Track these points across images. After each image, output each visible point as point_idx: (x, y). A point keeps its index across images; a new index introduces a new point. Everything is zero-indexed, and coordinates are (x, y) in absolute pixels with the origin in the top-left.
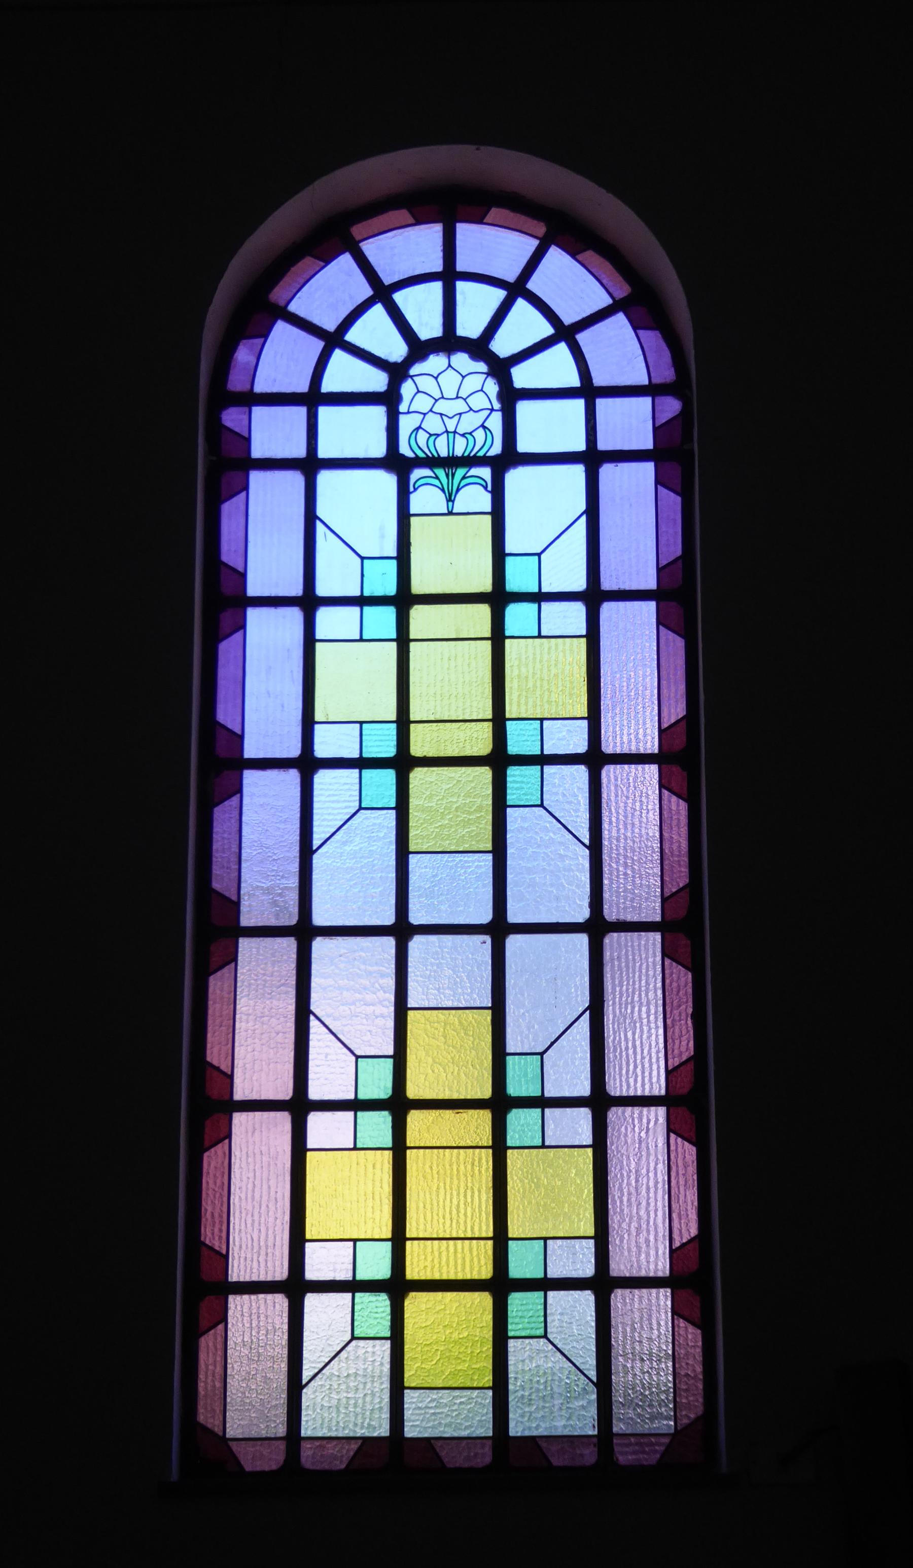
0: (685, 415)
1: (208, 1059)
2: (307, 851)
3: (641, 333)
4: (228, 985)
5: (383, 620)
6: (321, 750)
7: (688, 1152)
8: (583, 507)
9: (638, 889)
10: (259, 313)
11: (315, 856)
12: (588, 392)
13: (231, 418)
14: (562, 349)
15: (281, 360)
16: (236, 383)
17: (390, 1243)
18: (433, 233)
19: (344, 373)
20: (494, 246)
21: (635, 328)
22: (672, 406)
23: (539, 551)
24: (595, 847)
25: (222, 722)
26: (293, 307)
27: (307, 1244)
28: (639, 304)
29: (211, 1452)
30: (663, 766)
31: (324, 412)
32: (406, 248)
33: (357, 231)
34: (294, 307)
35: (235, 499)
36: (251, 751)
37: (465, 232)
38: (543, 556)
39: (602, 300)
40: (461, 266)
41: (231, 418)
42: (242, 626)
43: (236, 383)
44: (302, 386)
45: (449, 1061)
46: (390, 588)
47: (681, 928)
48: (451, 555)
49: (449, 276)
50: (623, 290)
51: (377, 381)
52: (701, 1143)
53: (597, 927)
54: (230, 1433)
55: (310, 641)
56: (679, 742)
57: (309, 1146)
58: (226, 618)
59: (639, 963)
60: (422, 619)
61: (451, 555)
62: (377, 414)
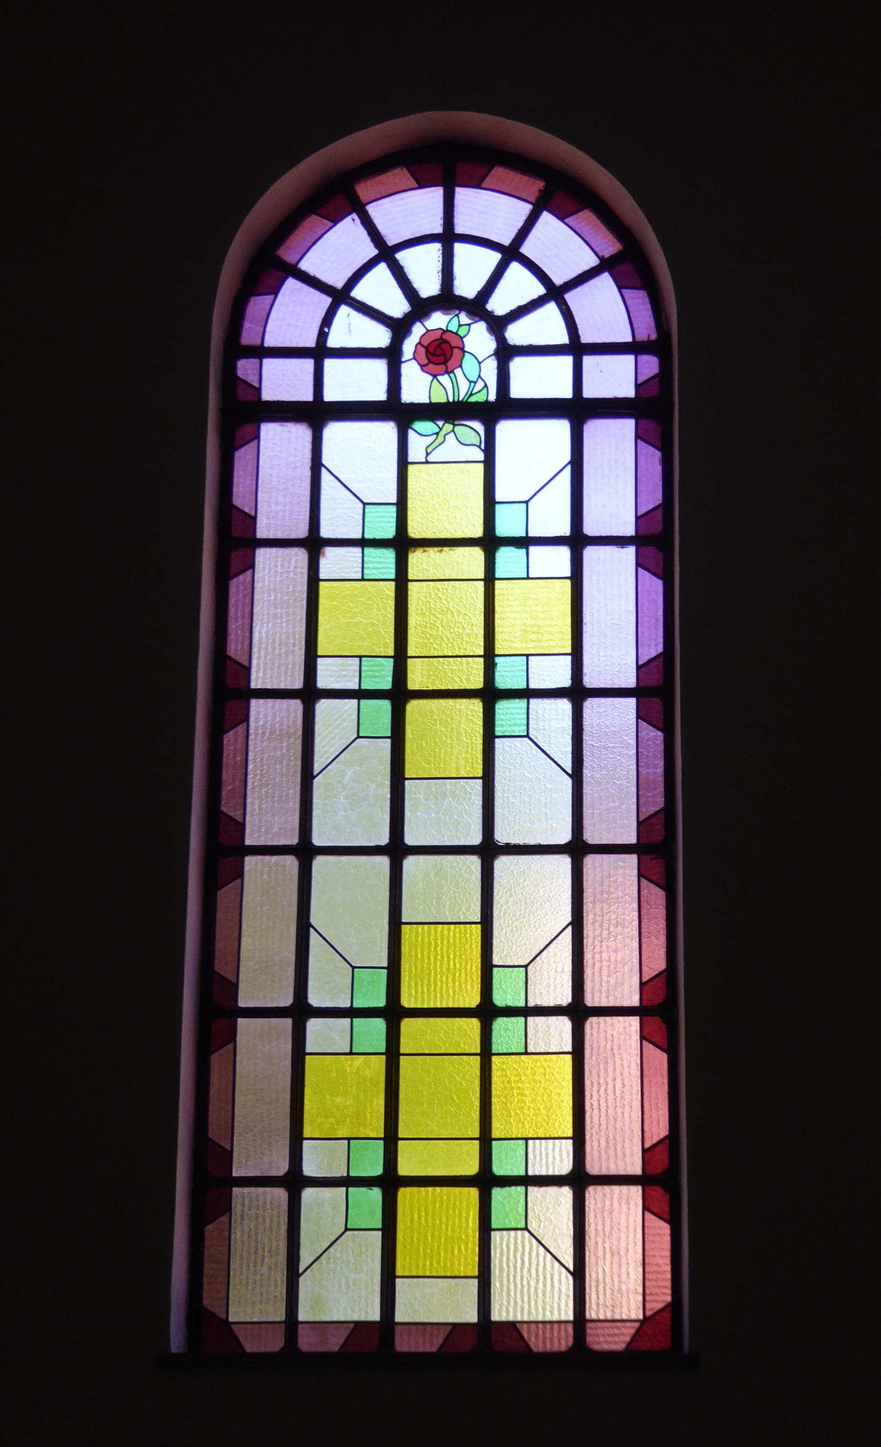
0: (664, 375)
1: (216, 969)
2: (307, 776)
3: (627, 293)
4: (251, 456)
5: (383, 561)
6: (324, 681)
7: (659, 1059)
8: (568, 458)
9: (616, 818)
10: (271, 269)
11: (301, 1279)
12: (577, 348)
13: (245, 368)
14: (552, 308)
15: (290, 315)
16: (248, 337)
17: (384, 1057)
18: (434, 196)
19: (350, 328)
20: (489, 210)
21: (620, 288)
22: (651, 365)
23: (527, 499)
24: (579, 1274)
25: (233, 656)
26: (304, 265)
27: (307, 1057)
28: (626, 266)
29: (210, 1328)
30: (646, 1188)
31: (330, 364)
32: (410, 210)
33: (363, 190)
34: (305, 265)
35: (223, 1050)
36: (263, 531)
37: (463, 195)
38: (530, 503)
39: (590, 261)
40: (460, 229)
41: (245, 368)
42: (251, 565)
43: (248, 337)
44: (309, 341)
45: (445, 734)
46: (389, 532)
47: (653, 848)
48: (446, 499)
49: (448, 238)
50: (611, 246)
51: (381, 337)
52: (669, 887)
53: (577, 849)
54: (231, 1319)
55: (299, 1053)
56: (661, 1162)
57: (319, 653)
58: (236, 557)
59: (617, 880)
60: (420, 562)
61: (446, 499)
62: (380, 367)
